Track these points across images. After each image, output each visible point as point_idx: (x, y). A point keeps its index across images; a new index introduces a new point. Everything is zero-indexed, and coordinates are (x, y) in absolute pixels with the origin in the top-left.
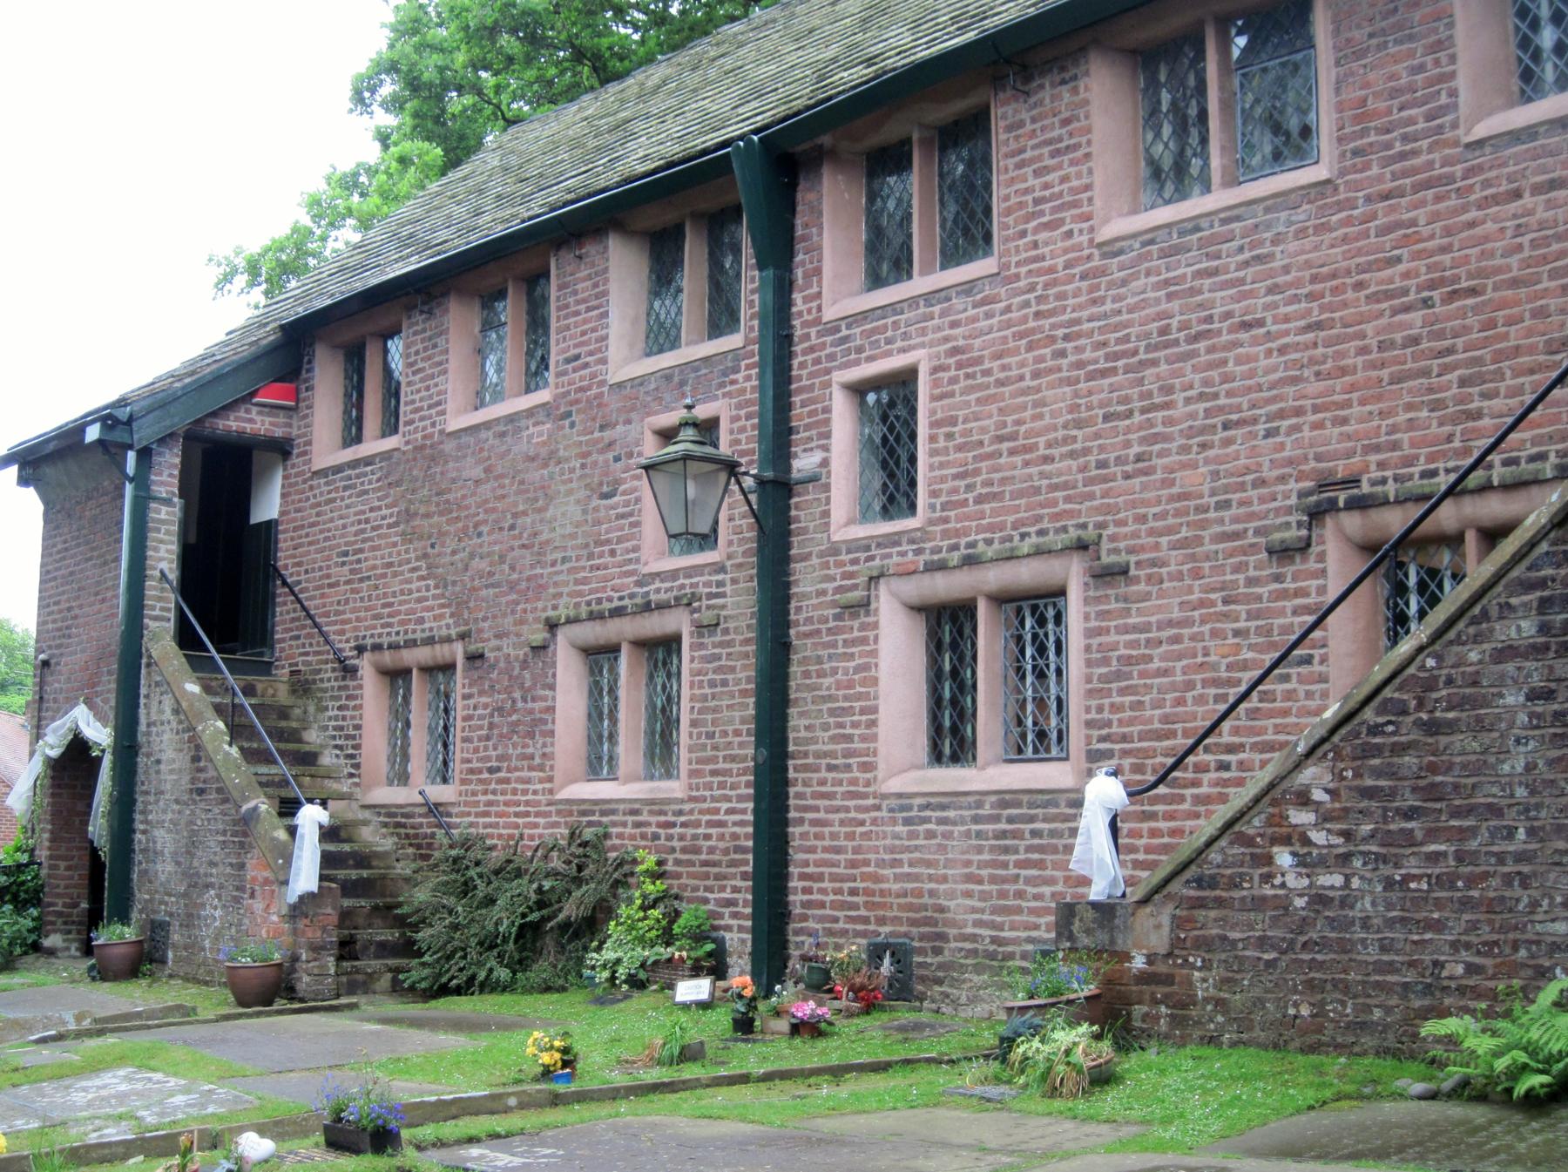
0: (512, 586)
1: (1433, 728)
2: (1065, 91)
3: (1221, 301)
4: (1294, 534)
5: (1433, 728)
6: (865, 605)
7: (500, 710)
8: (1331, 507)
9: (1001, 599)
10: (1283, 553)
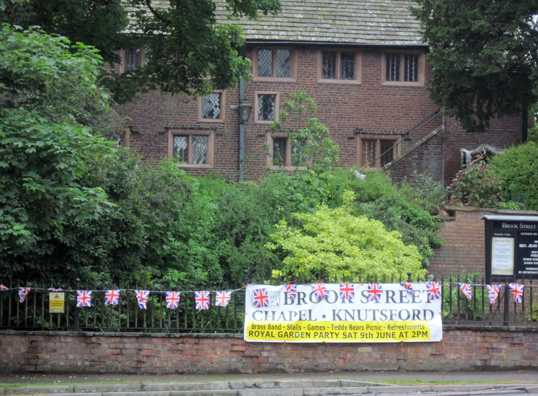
0: (150, 118)
1: (404, 167)
2: (312, 56)
3: (340, 98)
4: (352, 136)
5: (404, 167)
6: (264, 136)
7: (146, 146)
8: (359, 133)
9: (382, 141)
10: (350, 138)
